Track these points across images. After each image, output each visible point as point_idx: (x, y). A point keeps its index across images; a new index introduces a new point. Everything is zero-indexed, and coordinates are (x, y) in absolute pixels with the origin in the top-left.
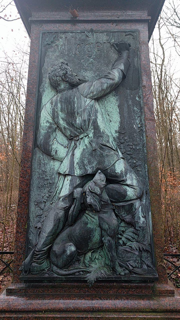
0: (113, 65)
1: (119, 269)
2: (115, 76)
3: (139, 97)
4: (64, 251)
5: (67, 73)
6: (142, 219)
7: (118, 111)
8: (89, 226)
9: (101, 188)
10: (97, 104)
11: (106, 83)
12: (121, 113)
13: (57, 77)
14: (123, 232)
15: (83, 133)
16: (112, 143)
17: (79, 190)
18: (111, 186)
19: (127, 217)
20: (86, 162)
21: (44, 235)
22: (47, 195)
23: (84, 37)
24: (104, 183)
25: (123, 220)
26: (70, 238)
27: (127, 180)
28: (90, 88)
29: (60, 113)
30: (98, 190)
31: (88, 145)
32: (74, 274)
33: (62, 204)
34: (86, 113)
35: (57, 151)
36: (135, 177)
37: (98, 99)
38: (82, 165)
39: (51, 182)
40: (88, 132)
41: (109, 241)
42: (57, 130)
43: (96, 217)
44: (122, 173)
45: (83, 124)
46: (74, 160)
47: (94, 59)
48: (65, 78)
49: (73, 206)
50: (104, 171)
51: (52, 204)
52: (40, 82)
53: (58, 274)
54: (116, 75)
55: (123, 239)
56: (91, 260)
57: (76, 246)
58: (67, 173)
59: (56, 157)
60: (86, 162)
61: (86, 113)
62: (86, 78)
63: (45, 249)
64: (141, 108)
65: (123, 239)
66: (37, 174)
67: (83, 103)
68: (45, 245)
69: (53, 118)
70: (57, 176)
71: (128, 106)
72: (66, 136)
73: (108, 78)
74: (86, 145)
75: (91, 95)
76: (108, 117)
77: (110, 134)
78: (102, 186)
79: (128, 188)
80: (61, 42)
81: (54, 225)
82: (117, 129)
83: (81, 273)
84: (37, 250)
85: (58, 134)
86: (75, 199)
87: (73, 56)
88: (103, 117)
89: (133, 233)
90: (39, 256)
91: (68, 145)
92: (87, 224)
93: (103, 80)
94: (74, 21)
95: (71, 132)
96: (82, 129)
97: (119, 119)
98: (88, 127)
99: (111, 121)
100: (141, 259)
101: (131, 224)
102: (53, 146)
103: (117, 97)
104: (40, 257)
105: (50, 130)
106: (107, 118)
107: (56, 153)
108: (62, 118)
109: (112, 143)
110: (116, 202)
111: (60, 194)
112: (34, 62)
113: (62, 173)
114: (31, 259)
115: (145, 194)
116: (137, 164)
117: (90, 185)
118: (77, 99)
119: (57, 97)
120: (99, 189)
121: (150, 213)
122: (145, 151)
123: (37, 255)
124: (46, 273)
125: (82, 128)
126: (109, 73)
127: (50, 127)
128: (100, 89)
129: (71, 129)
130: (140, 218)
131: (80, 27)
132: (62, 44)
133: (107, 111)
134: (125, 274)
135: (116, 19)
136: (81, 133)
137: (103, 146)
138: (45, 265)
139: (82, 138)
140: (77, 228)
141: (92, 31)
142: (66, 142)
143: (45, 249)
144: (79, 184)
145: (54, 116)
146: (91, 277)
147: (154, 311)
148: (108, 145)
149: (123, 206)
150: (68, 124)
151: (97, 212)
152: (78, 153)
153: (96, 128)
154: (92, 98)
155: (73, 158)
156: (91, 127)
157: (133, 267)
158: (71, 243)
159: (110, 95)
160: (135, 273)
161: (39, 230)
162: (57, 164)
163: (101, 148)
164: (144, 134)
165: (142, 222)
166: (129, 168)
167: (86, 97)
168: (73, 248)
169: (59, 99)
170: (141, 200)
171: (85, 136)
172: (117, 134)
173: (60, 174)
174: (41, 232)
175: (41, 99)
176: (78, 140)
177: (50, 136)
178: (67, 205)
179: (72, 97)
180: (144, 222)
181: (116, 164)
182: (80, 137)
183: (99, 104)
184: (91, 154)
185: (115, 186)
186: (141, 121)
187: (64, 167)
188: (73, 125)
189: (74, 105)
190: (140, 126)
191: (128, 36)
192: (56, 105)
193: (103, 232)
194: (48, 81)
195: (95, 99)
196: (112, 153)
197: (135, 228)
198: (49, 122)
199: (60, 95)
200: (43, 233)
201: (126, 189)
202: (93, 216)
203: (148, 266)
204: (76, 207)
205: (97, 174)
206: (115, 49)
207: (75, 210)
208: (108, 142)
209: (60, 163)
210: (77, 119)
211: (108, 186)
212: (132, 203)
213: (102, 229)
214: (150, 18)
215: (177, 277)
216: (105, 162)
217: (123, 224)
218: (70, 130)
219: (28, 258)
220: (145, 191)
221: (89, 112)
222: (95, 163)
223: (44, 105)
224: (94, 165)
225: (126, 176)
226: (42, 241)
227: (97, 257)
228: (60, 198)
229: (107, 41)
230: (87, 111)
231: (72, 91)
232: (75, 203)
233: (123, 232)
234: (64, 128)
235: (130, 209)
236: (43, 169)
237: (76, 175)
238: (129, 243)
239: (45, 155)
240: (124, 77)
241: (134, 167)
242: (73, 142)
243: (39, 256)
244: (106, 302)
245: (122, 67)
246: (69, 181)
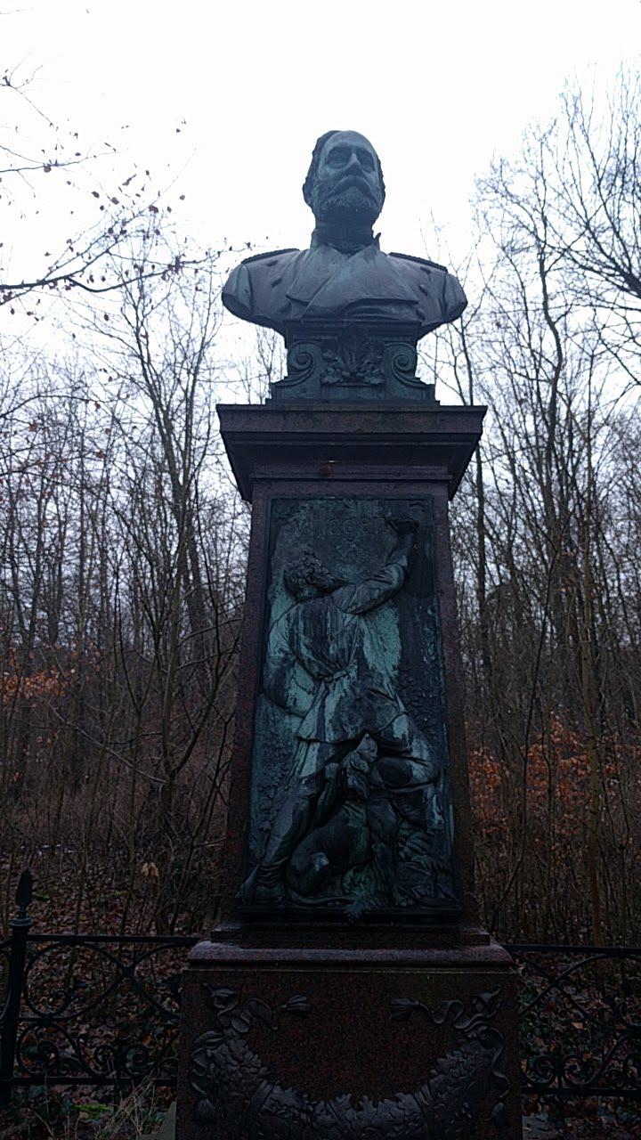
0: (390, 556)
1: (399, 897)
2: (391, 577)
3: (433, 611)
4: (311, 865)
5: (314, 572)
6: (438, 817)
7: (397, 631)
8: (350, 824)
9: (369, 763)
10: (362, 621)
11: (378, 589)
12: (403, 636)
13: (299, 578)
14: (407, 838)
15: (339, 670)
16: (388, 688)
17: (334, 765)
18: (386, 760)
19: (413, 813)
20: (345, 719)
21: (277, 842)
22: (279, 775)
23: (340, 508)
24: (374, 754)
25: (405, 818)
26: (320, 846)
27: (411, 750)
28: (351, 597)
29: (303, 636)
30: (365, 766)
31: (348, 690)
32: (325, 904)
33: (304, 790)
34: (344, 639)
35: (296, 699)
36: (425, 746)
37: (367, 612)
38: (338, 723)
39: (285, 753)
40: (348, 669)
41: (382, 849)
42: (296, 664)
43: (362, 811)
44: (404, 738)
45: (340, 656)
46: (326, 714)
47: (358, 545)
48: (311, 580)
49: (324, 793)
50: (375, 735)
51: (287, 790)
52: (268, 581)
53: (304, 904)
54: (394, 575)
55: (406, 850)
56: (353, 884)
57: (328, 857)
58: (313, 737)
59: (294, 710)
60: (345, 719)
61: (344, 639)
62: (345, 576)
63: (279, 862)
64: (436, 629)
65: (406, 850)
66: (262, 737)
67: (341, 621)
68: (278, 856)
69: (291, 644)
70: (296, 743)
71: (414, 624)
72: (309, 673)
73: (381, 581)
74: (345, 691)
75: (354, 608)
76: (381, 643)
77: (383, 672)
78: (372, 760)
79: (414, 764)
80: (302, 516)
81: (293, 824)
82: (396, 663)
83: (337, 903)
84: (266, 865)
85: (297, 671)
86: (326, 780)
87: (323, 538)
88: (372, 643)
89: (422, 839)
90: (270, 874)
91: (314, 688)
92: (347, 821)
93: (373, 584)
94: (323, 478)
95: (320, 667)
96: (340, 664)
97: (399, 647)
98: (349, 659)
99: (385, 650)
100: (435, 885)
101: (420, 825)
102: (290, 692)
103: (396, 609)
104: (270, 876)
105: (285, 665)
106: (379, 645)
107: (295, 703)
108: (305, 645)
109: (388, 688)
110: (392, 788)
111: (300, 772)
112: (258, 547)
113: (304, 737)
114: (255, 880)
115: (442, 775)
116: (430, 724)
117: (352, 758)
118: (331, 614)
119: (297, 609)
120: (366, 764)
121: (451, 807)
122: (443, 702)
123: (266, 873)
124: (280, 903)
125: (337, 662)
126: (383, 572)
127: (285, 660)
128: (368, 599)
129: (320, 662)
130: (433, 816)
131: (337, 488)
132: (304, 518)
133: (378, 632)
134: (408, 906)
135: (395, 478)
136: (336, 670)
137: (373, 694)
138: (277, 890)
139: (337, 679)
140: (331, 829)
141: (354, 497)
142: (310, 684)
143: (279, 862)
144: (333, 756)
145: (293, 641)
146: (353, 910)
147: (455, 964)
148: (381, 690)
149: (405, 795)
150: (314, 654)
151: (364, 801)
152: (331, 704)
153: (362, 661)
154: (354, 613)
155: (323, 711)
156: (353, 660)
157: (422, 896)
158: (321, 853)
159: (385, 607)
160: (426, 905)
161: (268, 834)
162: (296, 721)
163: (370, 696)
164: (441, 673)
165: (436, 822)
166: (415, 729)
167: (345, 612)
168: (325, 861)
169: (300, 612)
170: (436, 786)
171: (344, 676)
172: (396, 672)
173: (300, 739)
174: (272, 836)
175: (270, 611)
176: (332, 681)
177: (285, 675)
178: (315, 792)
179: (323, 612)
180: (440, 822)
181: (395, 724)
182: (335, 677)
183: (366, 621)
184: (353, 707)
185: (394, 760)
186: (435, 649)
187: (308, 727)
188: (324, 657)
189: (326, 625)
190: (433, 658)
191: (414, 507)
192: (296, 623)
193: (373, 834)
194: (281, 580)
195: (359, 614)
196: (388, 704)
197: (425, 832)
198: (284, 652)
199: (302, 606)
200: (276, 838)
201: (411, 766)
202: (357, 808)
203: (446, 895)
204: (329, 794)
205: (364, 739)
206: (394, 529)
207: (327, 799)
208: (381, 685)
209: (300, 720)
210: (331, 648)
211: (381, 760)
212: (420, 790)
213: (371, 830)
214: (451, 477)
215: (568, 1030)
216: (375, 719)
217: (405, 825)
218: (318, 664)
219: (250, 880)
220: (442, 770)
221: (350, 637)
222: (361, 720)
223: (274, 619)
224: (358, 725)
225: (411, 744)
226: (274, 850)
227: (363, 880)
228: (301, 780)
229: (380, 514)
230: (346, 634)
231: (323, 601)
232: (326, 788)
233: (407, 838)
234: (309, 661)
235: (418, 799)
236: (273, 730)
237: (327, 740)
238: (415, 858)
239: (275, 707)
240: (407, 575)
241: (422, 728)
242: (323, 684)
243: (270, 874)
244: (379, 952)
245: (404, 562)
246: (316, 752)
